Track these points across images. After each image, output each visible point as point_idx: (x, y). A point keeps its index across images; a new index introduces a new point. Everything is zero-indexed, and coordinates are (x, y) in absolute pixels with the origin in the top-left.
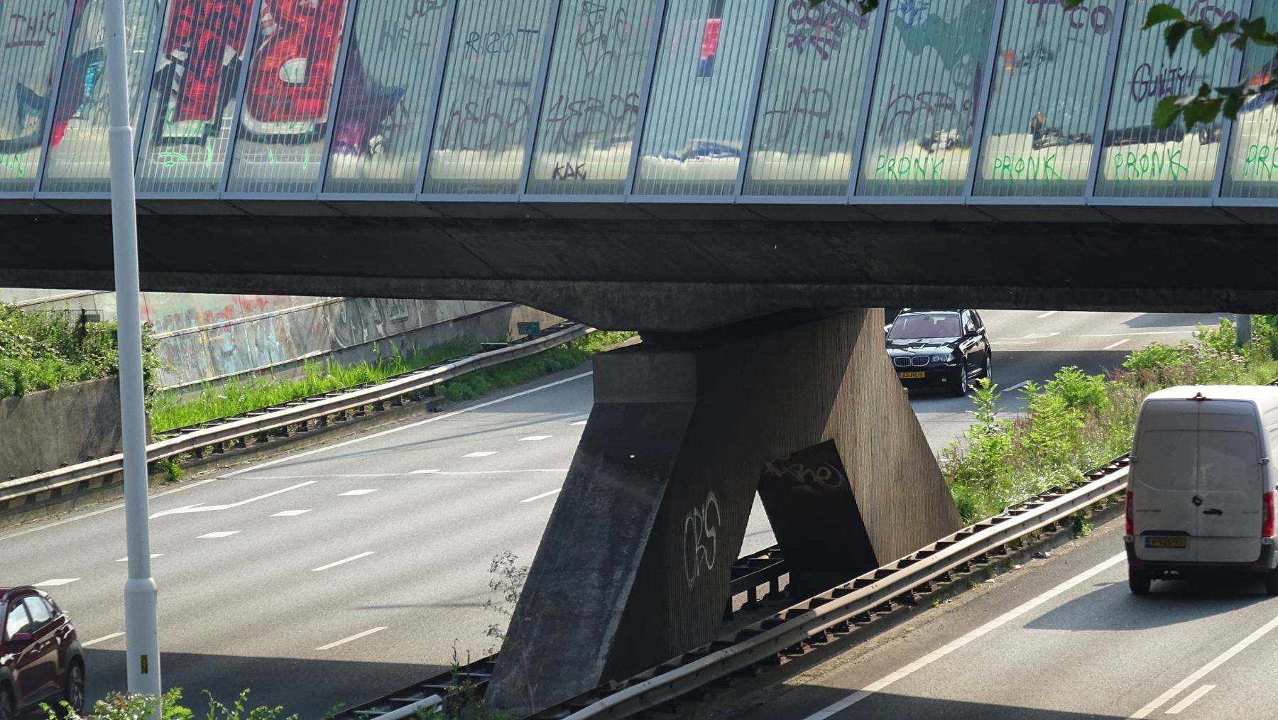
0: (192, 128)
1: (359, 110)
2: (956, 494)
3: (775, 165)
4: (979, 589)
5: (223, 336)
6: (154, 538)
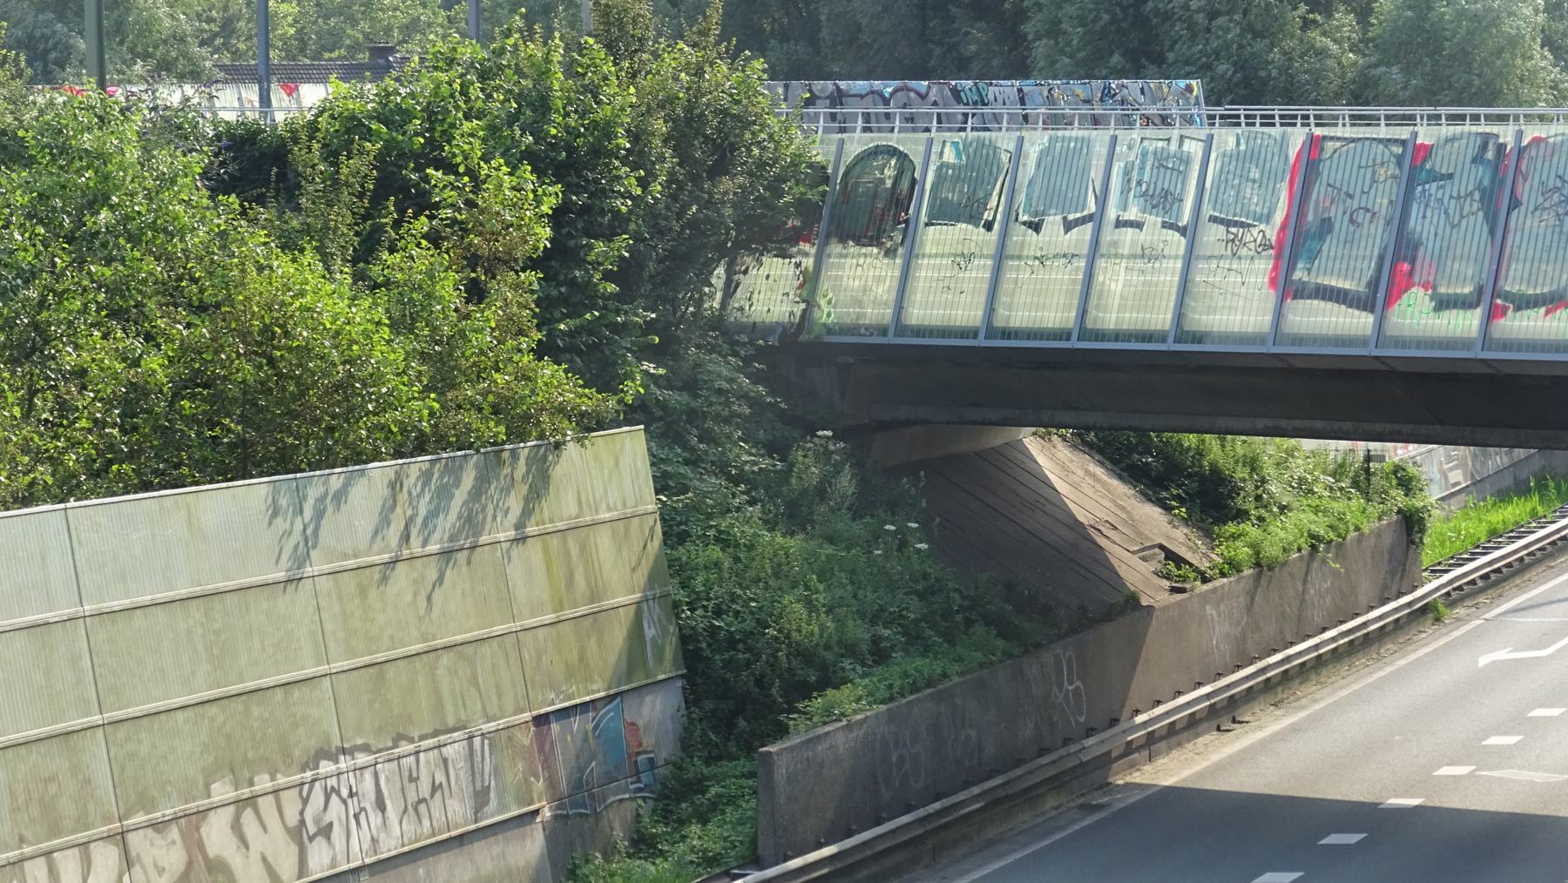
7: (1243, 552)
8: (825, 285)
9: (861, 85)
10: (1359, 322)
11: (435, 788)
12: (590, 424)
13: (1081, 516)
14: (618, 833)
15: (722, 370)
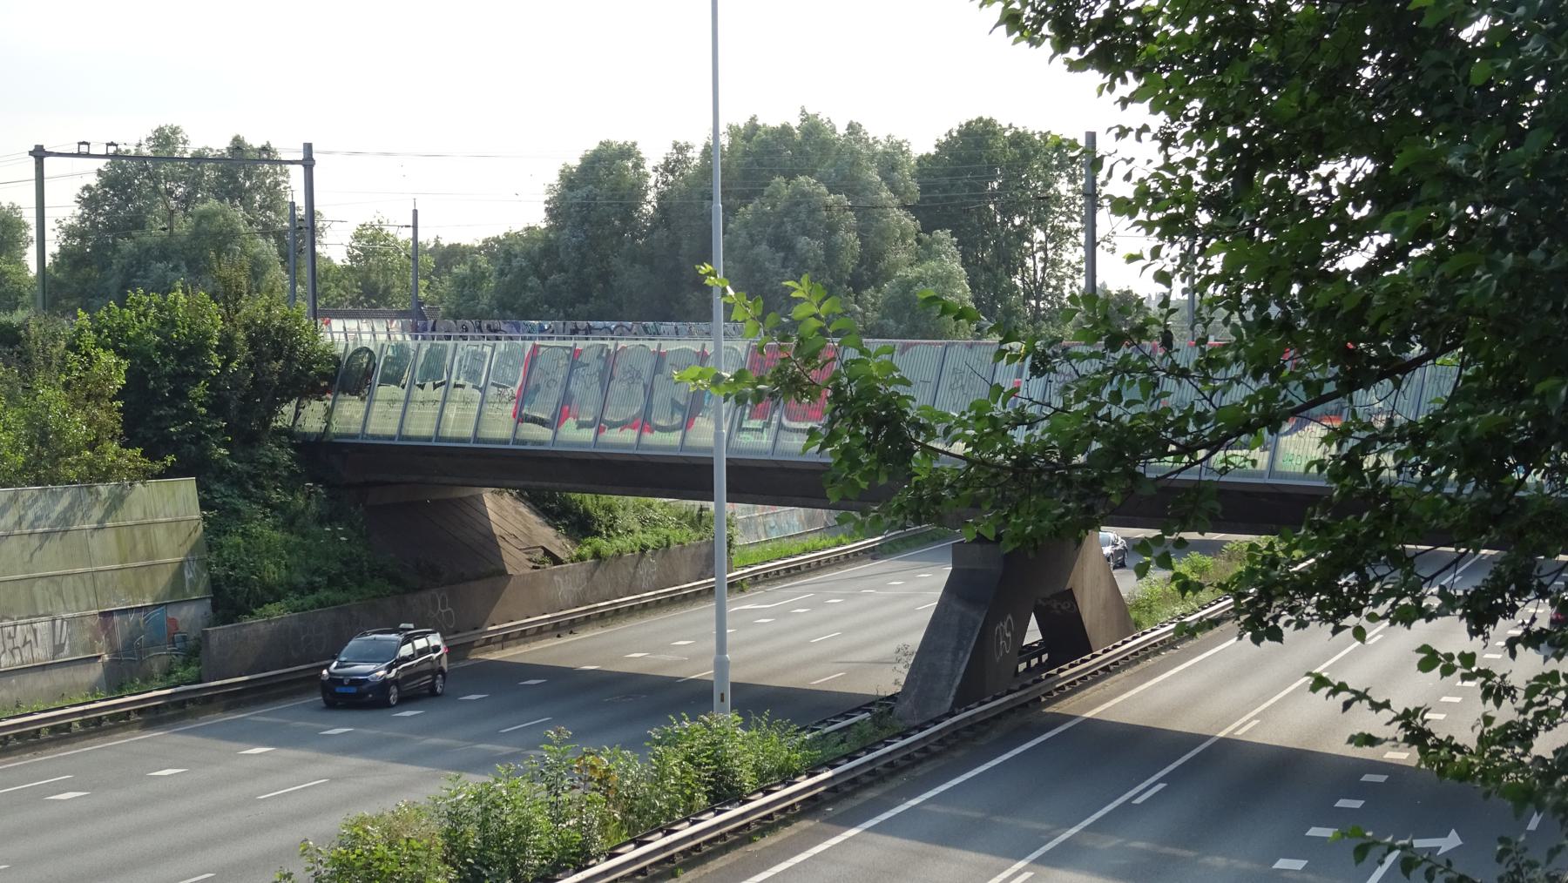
0: (756, 423)
2: (1134, 615)
4: (1144, 664)
5: (770, 519)
6: (728, 622)
7: (586, 550)
8: (335, 414)
9: (599, 324)
10: (545, 434)
11: (25, 643)
13: (497, 530)
14: (156, 669)
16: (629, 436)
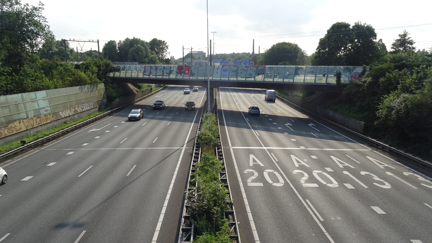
1: (192, 74)
3: (222, 79)
10: (161, 77)
12: (100, 83)
15: (109, 80)
16: (161, 77)
